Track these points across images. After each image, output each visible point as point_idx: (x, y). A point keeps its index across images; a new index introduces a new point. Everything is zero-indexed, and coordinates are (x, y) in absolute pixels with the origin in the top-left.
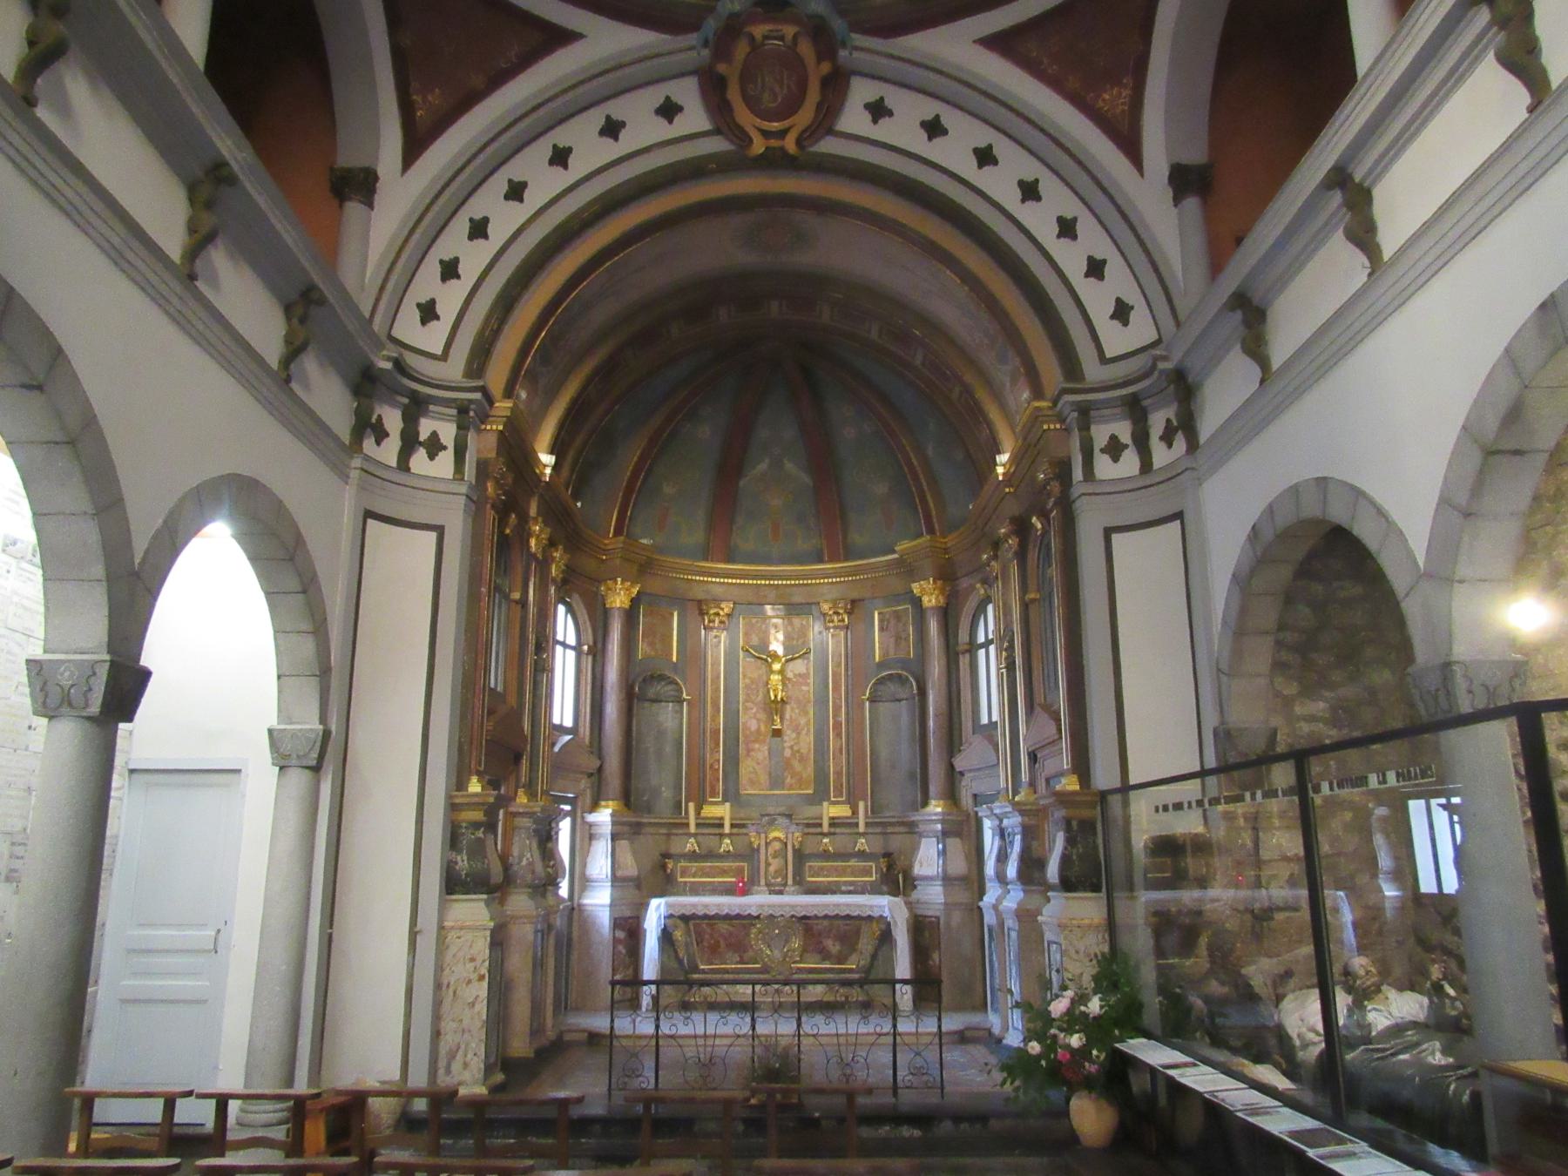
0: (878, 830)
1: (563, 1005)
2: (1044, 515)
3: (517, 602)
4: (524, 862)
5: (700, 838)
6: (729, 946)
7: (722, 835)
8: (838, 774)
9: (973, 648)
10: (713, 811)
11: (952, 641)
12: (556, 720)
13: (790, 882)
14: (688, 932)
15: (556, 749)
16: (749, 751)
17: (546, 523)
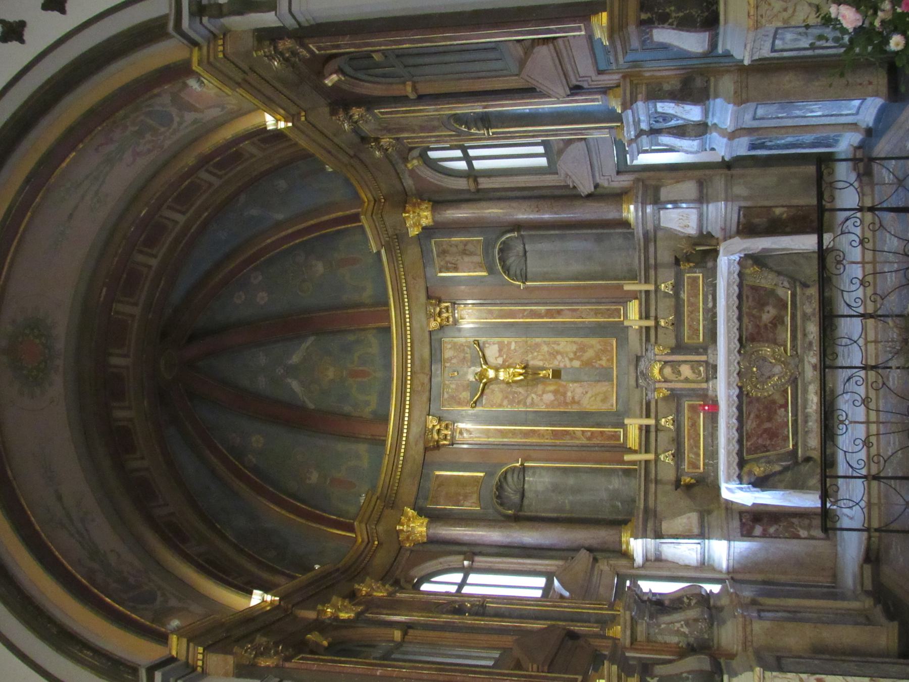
0: (652, 272)
1: (833, 592)
2: (321, 64)
3: (405, 634)
4: (685, 630)
5: (659, 451)
6: (769, 419)
7: (658, 428)
8: (597, 313)
9: (472, 174)
10: (633, 437)
11: (467, 196)
12: (538, 594)
13: (704, 358)
14: (757, 460)
15: (567, 594)
16: (574, 402)
17: (326, 601)
